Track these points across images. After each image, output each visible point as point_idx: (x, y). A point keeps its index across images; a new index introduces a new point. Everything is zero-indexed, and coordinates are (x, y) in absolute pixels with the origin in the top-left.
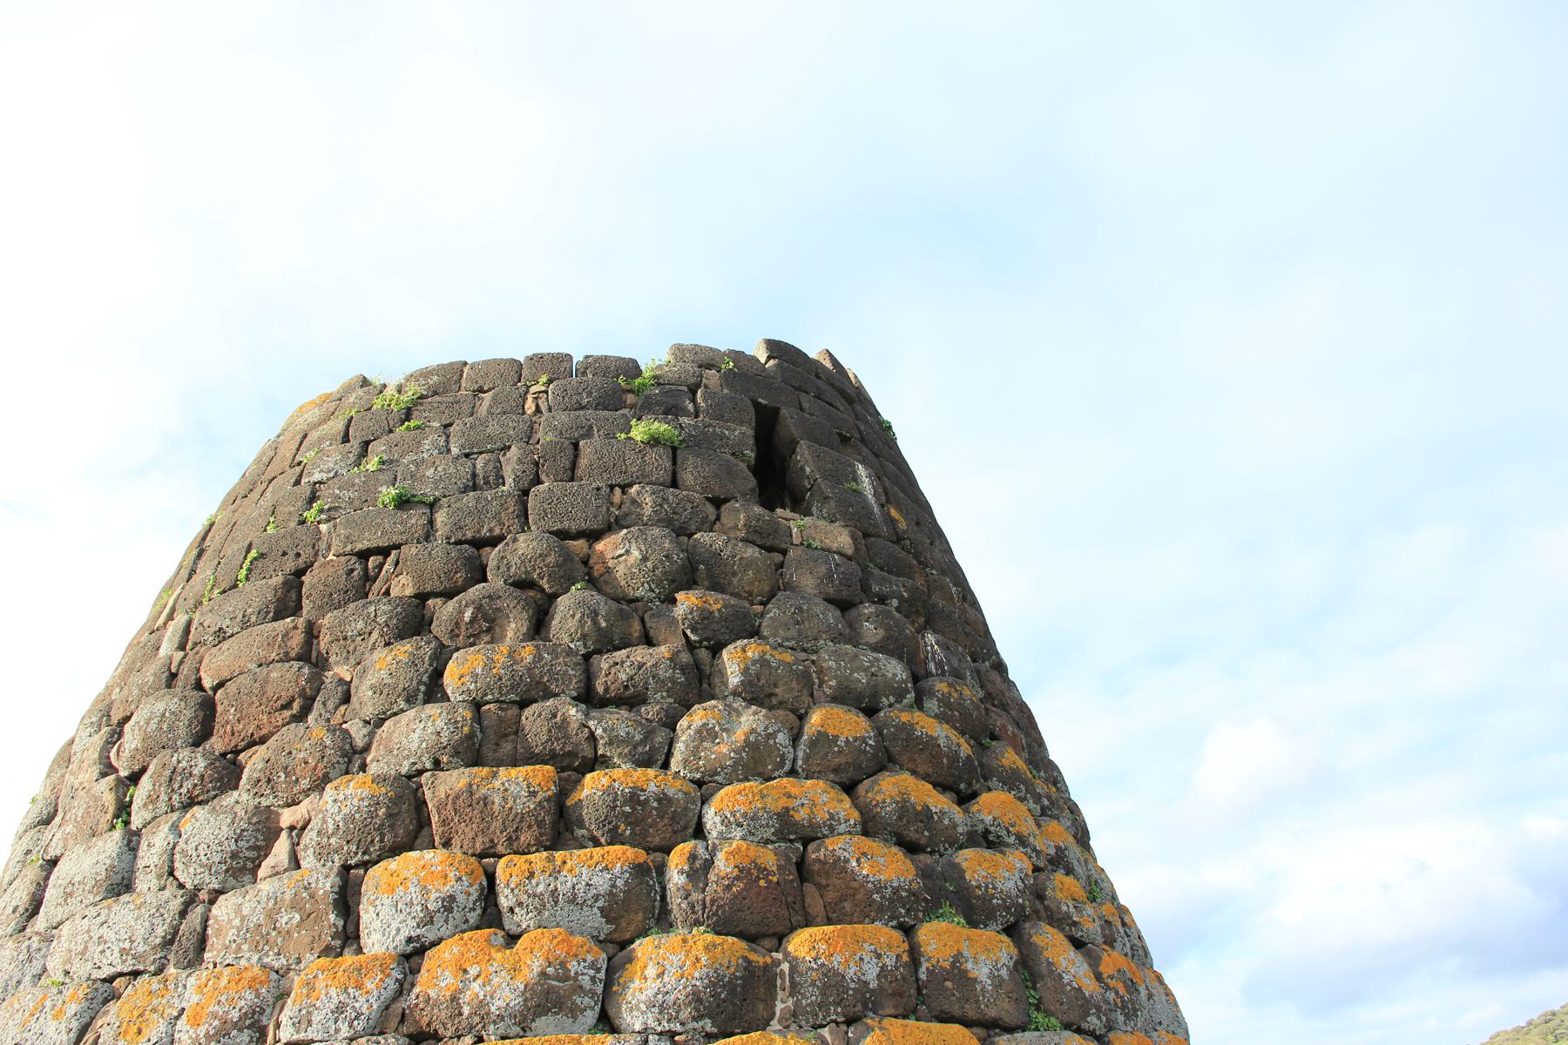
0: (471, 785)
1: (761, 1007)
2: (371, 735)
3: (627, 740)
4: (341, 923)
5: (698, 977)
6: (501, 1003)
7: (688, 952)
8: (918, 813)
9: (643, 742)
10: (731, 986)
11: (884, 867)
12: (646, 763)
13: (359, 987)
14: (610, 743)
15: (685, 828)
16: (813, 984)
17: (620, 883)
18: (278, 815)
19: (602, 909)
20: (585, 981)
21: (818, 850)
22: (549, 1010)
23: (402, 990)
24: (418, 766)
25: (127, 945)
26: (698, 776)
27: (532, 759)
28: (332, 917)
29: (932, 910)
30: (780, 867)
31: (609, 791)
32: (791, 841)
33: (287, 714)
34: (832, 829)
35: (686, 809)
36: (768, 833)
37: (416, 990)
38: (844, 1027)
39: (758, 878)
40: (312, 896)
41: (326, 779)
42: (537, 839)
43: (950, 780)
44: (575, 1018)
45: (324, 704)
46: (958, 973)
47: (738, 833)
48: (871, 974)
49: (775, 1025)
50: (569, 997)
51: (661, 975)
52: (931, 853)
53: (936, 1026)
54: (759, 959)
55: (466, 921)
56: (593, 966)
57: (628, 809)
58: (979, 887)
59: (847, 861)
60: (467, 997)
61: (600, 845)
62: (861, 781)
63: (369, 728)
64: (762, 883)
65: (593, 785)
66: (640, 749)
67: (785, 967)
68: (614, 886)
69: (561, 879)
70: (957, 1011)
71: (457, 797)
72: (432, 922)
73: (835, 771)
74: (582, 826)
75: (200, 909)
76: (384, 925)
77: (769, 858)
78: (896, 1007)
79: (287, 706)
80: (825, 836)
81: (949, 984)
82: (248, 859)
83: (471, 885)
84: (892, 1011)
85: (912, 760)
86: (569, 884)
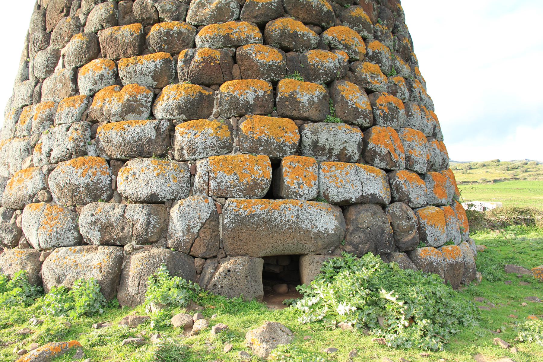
0: (111, 34)
1: (206, 110)
2: (86, 19)
3: (170, 11)
4: (74, 86)
5: (180, 99)
6: (114, 110)
7: (178, 90)
8: (290, 34)
9: (176, 11)
10: (193, 103)
11: (270, 56)
12: (177, 19)
13: (74, 106)
14: (163, 12)
15: (188, 44)
16: (226, 102)
17: (158, 66)
18: (61, 51)
19: (152, 76)
20: (143, 102)
21: (239, 51)
22: (130, 112)
23: (87, 107)
24: (97, 29)
25: (22, 97)
26: (196, 23)
27: (136, 21)
28: (71, 84)
29: (288, 74)
30: (221, 58)
31: (159, 31)
32: (230, 47)
33: (63, 14)
34: (247, 42)
35: (188, 36)
36: (220, 44)
37: (91, 107)
38: (238, 118)
39: (211, 62)
40: (65, 78)
41: (72, 36)
42: (133, 52)
43: (317, 21)
44: (140, 115)
45: (73, 9)
46: (292, 99)
47: (207, 45)
48: (251, 98)
49: (212, 117)
50: (137, 108)
51: (168, 99)
52: (297, 51)
53: (280, 119)
54: (206, 93)
55: (109, 83)
56: (146, 96)
57: (165, 38)
58: (314, 65)
59: (251, 54)
60: (104, 109)
61: (156, 52)
62: (268, 22)
63: (85, 16)
64: (212, 64)
65: (154, 30)
66: (174, 14)
67: (219, 96)
68: (156, 67)
69: (138, 66)
70: (289, 113)
71: (107, 39)
72: (96, 84)
73: (255, 17)
74: (150, 46)
75: (39, 85)
76: (85, 85)
77: (217, 54)
78: (261, 111)
79: (62, 11)
80: (244, 45)
81: (287, 103)
82: (52, 67)
83: (109, 70)
84: (259, 113)
85: (296, 12)
86: (140, 68)
